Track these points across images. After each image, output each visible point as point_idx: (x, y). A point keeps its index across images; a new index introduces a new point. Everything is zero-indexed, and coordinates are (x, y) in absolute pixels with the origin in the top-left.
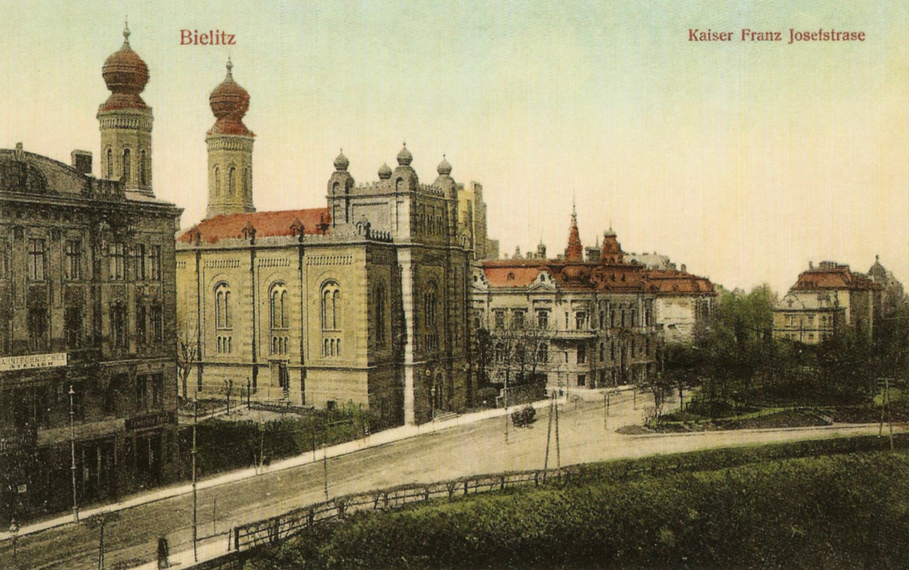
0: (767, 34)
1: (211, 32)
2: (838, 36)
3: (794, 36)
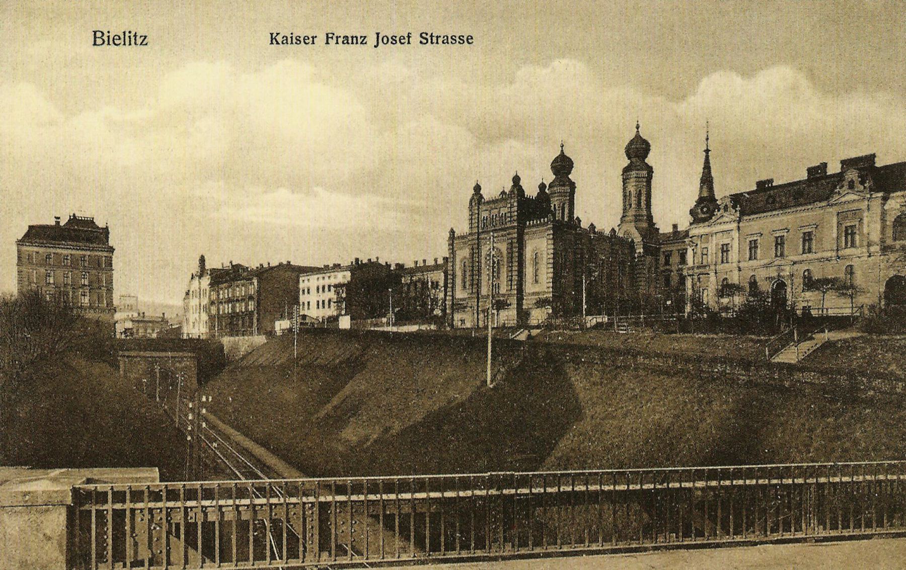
0: (352, 37)
1: (124, 33)
2: (437, 40)
3: (426, 38)
